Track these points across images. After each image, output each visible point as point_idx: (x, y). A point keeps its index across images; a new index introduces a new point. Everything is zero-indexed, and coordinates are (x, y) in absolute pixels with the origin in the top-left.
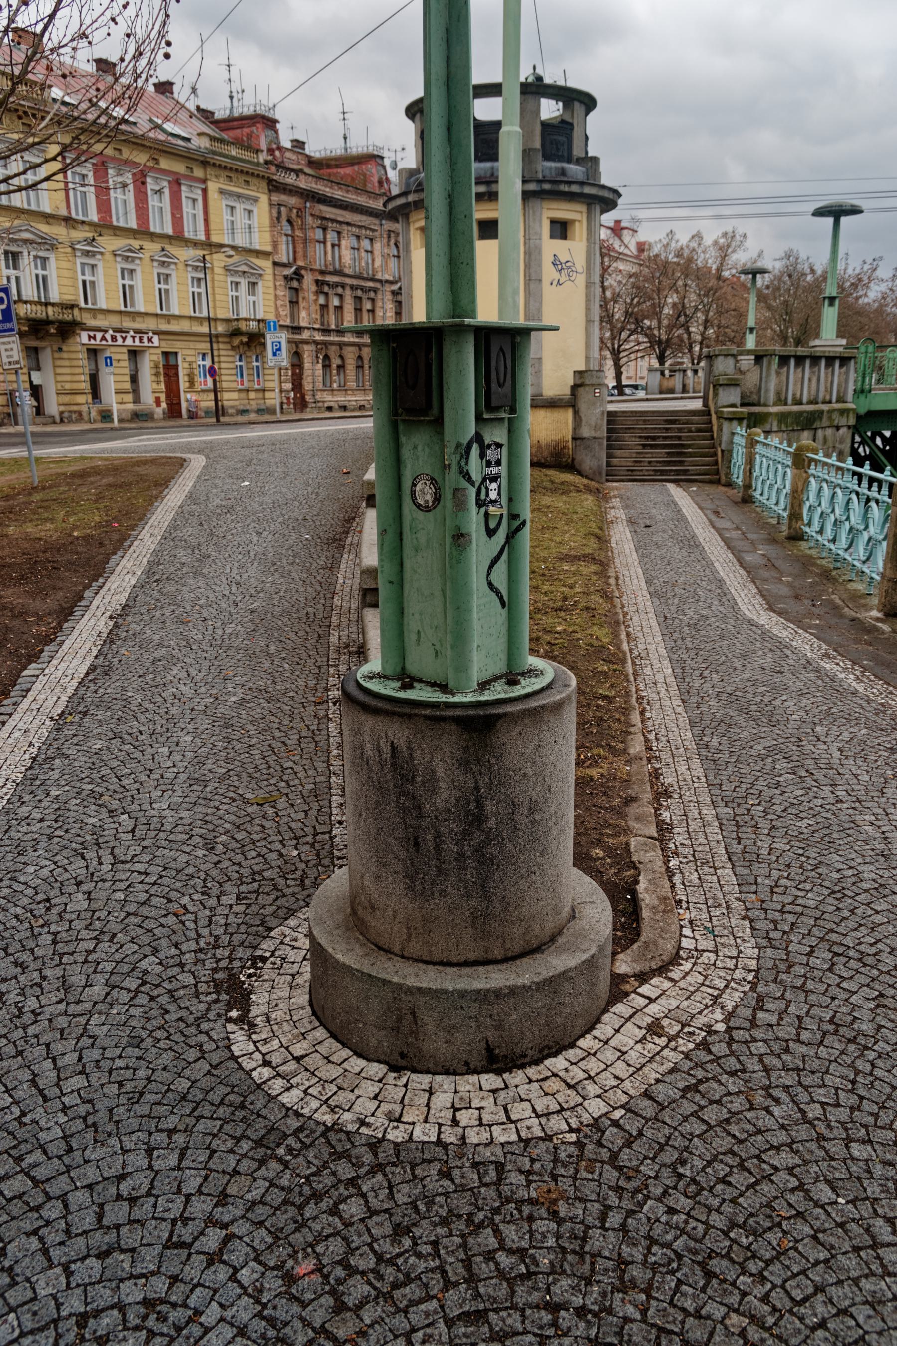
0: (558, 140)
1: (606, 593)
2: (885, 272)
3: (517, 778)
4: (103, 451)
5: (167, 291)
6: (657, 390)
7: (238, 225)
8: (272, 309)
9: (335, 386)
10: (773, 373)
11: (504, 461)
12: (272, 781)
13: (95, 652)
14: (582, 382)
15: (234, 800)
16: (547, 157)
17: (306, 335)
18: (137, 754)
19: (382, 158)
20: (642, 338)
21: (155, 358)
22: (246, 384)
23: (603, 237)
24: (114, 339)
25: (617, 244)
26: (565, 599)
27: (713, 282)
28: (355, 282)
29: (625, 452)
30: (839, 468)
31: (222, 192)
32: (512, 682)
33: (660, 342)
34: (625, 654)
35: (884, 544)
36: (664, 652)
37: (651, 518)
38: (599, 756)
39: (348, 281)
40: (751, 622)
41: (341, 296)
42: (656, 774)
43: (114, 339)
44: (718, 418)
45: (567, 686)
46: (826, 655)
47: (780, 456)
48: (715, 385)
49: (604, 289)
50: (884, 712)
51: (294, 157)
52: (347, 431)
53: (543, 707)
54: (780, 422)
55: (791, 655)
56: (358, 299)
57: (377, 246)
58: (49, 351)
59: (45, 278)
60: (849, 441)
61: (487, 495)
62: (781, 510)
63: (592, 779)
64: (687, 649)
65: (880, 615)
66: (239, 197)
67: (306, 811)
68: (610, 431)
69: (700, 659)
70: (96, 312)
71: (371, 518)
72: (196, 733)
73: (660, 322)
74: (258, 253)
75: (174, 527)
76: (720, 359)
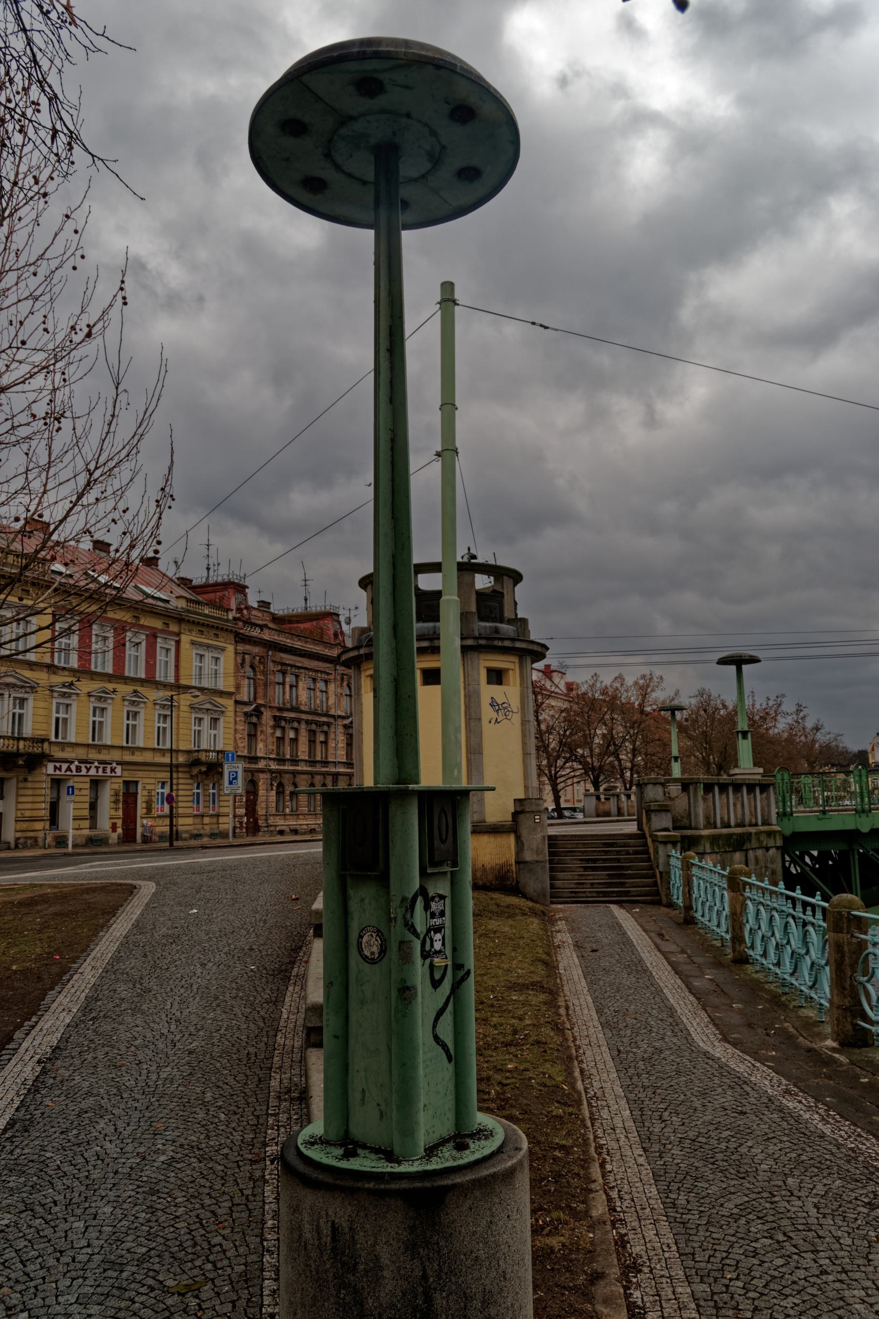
0: (490, 605)
1: (556, 1024)
2: (788, 706)
3: (468, 1263)
4: (54, 877)
5: (134, 726)
6: (593, 813)
7: (205, 671)
8: (232, 742)
9: (287, 811)
10: (700, 799)
11: (448, 913)
12: (198, 1263)
13: (17, 1104)
14: (522, 808)
15: (152, 1289)
16: (481, 619)
17: (261, 764)
18: (48, 1232)
19: (338, 615)
20: (576, 765)
21: (116, 786)
22: (202, 810)
23: (534, 678)
24: (78, 769)
25: (548, 684)
26: (515, 1032)
27: (637, 716)
28: (310, 717)
29: (568, 875)
30: (772, 892)
31: (193, 643)
32: (461, 1147)
33: (593, 769)
34: (579, 1093)
35: (827, 969)
36: (620, 1091)
37: (597, 942)
38: (559, 1220)
39: (304, 716)
40: (706, 1053)
41: (296, 730)
42: (622, 1242)
43: (78, 769)
44: (653, 841)
45: (518, 1149)
46: (787, 1092)
47: (716, 879)
48: (647, 810)
49: (539, 722)
50: (856, 1159)
51: (260, 615)
52: (297, 856)
53: (493, 1176)
54: (712, 844)
55: (752, 1093)
56: (312, 733)
57: (332, 687)
58: (14, 780)
59: (21, 716)
60: (779, 860)
61: (432, 946)
62: (723, 931)
63: (552, 1251)
64: (644, 1088)
65: (835, 1045)
66: (208, 646)
67: (233, 1302)
68: (551, 854)
69: (658, 1099)
70: (63, 746)
71: (318, 946)
72: (117, 1203)
73: (591, 750)
74: (221, 693)
75: (117, 958)
76: (650, 787)
